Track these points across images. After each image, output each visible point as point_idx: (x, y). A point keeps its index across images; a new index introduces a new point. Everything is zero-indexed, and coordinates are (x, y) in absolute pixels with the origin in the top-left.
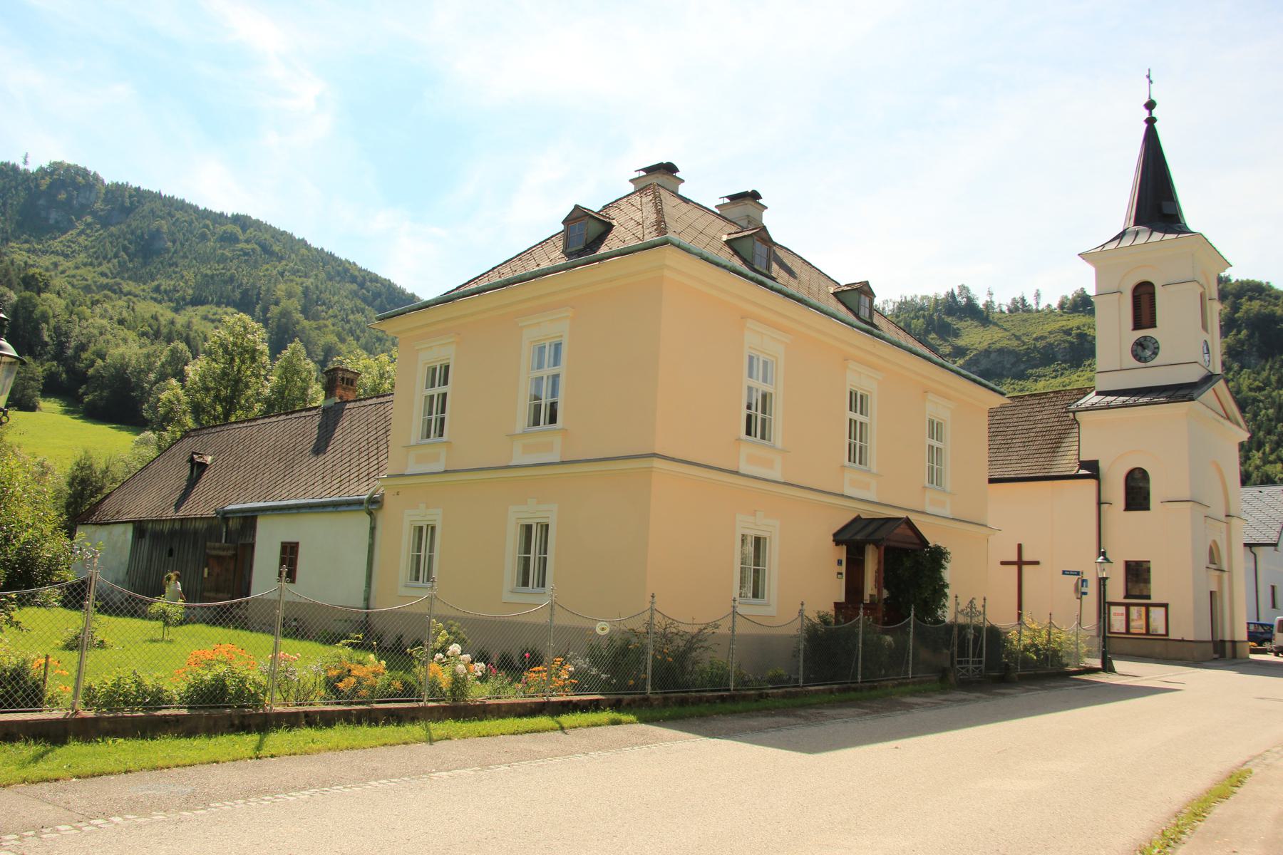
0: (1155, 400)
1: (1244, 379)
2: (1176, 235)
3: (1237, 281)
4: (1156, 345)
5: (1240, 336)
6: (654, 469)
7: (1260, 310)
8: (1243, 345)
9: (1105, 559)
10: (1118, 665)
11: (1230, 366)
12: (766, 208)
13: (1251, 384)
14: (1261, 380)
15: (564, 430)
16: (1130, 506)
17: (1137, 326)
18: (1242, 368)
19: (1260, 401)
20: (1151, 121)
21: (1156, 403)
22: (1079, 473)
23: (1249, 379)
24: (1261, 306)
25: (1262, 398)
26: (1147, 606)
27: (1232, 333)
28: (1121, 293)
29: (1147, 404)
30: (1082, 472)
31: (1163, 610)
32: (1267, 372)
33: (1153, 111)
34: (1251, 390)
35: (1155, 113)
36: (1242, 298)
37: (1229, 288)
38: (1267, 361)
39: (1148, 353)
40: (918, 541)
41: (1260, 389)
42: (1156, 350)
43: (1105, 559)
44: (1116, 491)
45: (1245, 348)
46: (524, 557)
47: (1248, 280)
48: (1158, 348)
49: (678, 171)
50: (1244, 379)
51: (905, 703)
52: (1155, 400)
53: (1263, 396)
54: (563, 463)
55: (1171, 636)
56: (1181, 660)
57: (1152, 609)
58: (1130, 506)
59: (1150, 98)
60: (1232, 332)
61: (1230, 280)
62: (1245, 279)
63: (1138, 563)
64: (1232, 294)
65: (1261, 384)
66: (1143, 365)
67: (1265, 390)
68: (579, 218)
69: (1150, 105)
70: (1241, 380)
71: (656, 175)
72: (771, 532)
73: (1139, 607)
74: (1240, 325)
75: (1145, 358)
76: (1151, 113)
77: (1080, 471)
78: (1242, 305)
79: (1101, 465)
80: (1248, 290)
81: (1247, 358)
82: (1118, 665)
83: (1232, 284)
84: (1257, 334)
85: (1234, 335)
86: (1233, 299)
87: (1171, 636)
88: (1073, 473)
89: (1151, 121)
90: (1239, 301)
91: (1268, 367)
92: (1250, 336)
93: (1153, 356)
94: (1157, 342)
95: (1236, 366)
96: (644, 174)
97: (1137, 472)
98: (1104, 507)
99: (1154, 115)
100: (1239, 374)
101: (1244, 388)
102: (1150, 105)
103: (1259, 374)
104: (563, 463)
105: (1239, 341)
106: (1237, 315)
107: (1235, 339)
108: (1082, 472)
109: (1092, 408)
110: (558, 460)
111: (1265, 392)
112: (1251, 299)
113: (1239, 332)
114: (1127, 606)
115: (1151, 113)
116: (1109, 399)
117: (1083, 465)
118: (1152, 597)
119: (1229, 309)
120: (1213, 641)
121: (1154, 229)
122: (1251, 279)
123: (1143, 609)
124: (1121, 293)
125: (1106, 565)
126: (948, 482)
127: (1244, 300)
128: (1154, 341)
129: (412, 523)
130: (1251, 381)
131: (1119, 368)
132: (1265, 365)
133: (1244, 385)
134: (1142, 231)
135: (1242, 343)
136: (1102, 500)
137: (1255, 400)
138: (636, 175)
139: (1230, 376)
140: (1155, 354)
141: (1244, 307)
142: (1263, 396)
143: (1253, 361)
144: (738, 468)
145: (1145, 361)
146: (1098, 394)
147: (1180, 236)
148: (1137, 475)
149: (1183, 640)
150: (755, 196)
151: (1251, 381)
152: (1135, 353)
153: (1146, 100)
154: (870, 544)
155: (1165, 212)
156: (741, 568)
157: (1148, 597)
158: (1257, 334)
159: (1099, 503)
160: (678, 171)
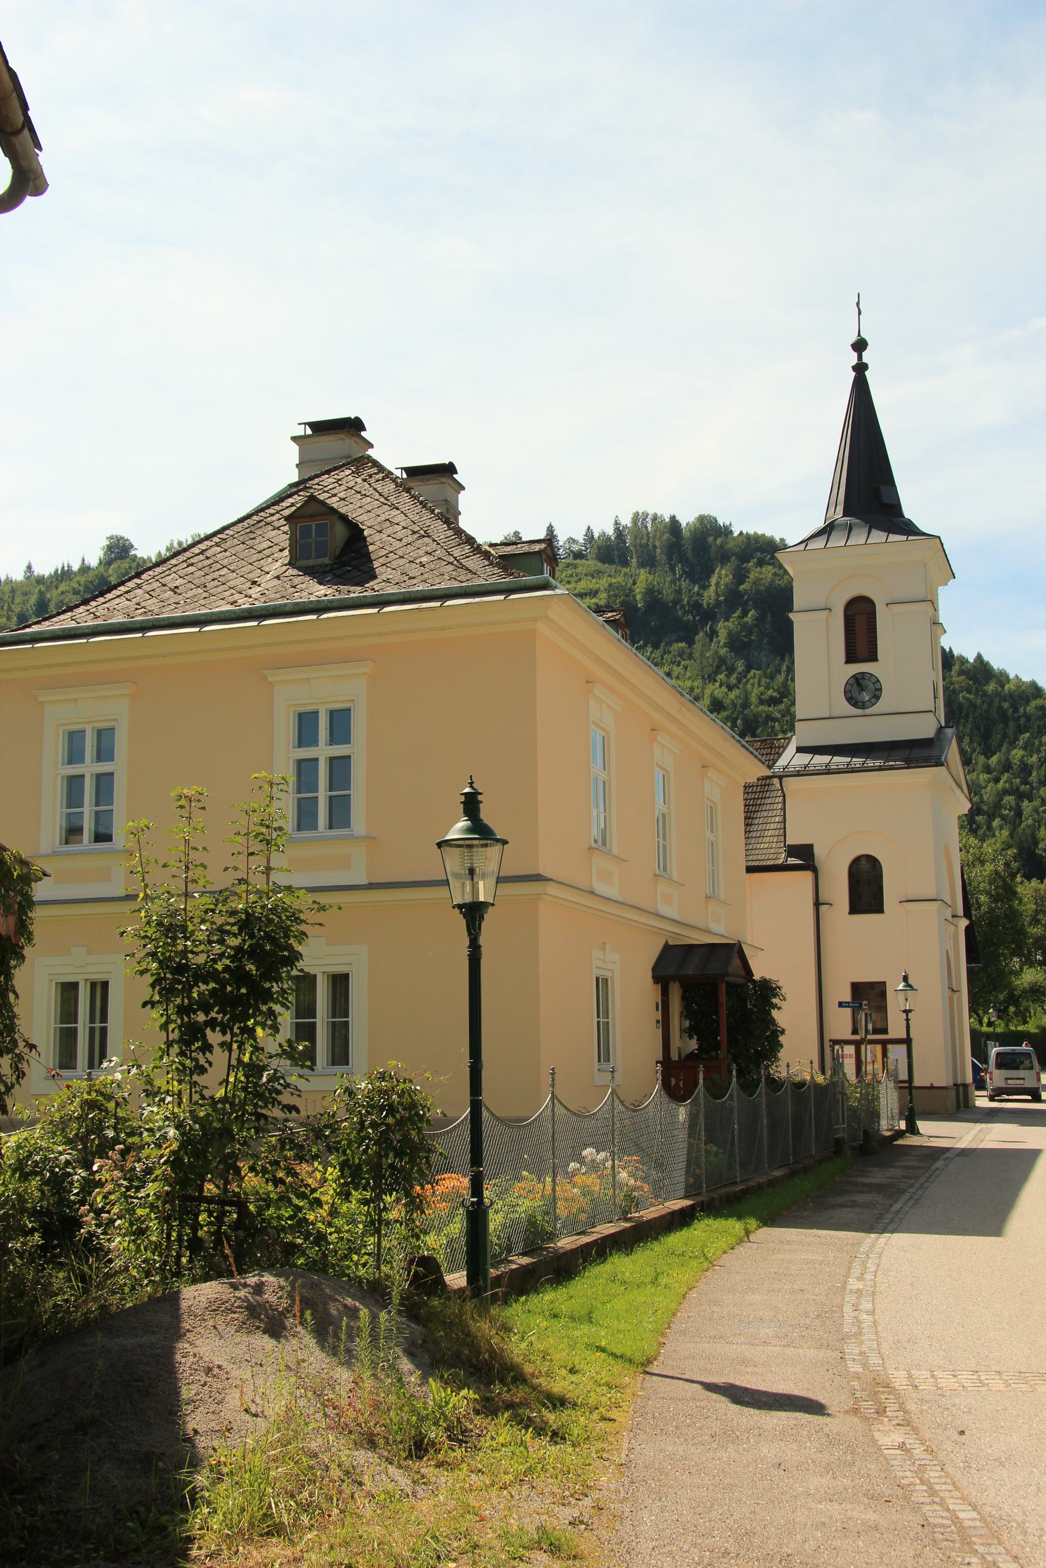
0: (890, 763)
1: (753, 685)
2: (904, 538)
3: (741, 533)
4: (877, 686)
5: (746, 619)
6: (543, 896)
7: (773, 581)
8: (751, 633)
9: (908, 985)
10: (922, 1125)
11: (733, 665)
12: (463, 488)
13: (762, 694)
14: (776, 687)
15: (370, 839)
16: (856, 908)
17: (851, 657)
18: (748, 668)
19: (774, 720)
20: (860, 368)
21: (892, 768)
22: (788, 863)
23: (759, 685)
24: (775, 574)
25: (778, 715)
26: (884, 1043)
27: (736, 615)
28: (830, 610)
29: (880, 769)
30: (792, 861)
31: (903, 1048)
32: (783, 675)
33: (864, 353)
34: (762, 702)
35: (866, 357)
36: (749, 562)
37: (731, 545)
38: (783, 659)
39: (866, 697)
40: (743, 973)
41: (773, 701)
42: (877, 693)
43: (908, 985)
44: (838, 889)
45: (753, 638)
46: (296, 1023)
47: (755, 533)
48: (881, 689)
49: (365, 430)
50: (753, 685)
51: (866, 1185)
52: (890, 763)
53: (779, 711)
54: (371, 886)
55: (917, 1083)
56: (929, 1114)
57: (889, 1046)
58: (856, 908)
59: (859, 335)
60: (735, 612)
61: (731, 532)
62: (751, 532)
63: (872, 985)
64: (735, 554)
65: (775, 694)
66: (859, 712)
67: (782, 702)
68: (316, 516)
69: (860, 346)
70: (749, 686)
71: (342, 436)
72: (613, 970)
73: (873, 1046)
74: (746, 602)
75: (863, 703)
76: (860, 357)
77: (789, 859)
78: (749, 573)
79: (816, 851)
80: (757, 550)
81: (756, 653)
82: (922, 1125)
83: (734, 539)
84: (769, 618)
85: (739, 617)
86: (736, 562)
87: (917, 1083)
88: (780, 862)
89: (860, 368)
90: (745, 565)
91: (784, 668)
92: (760, 620)
93: (873, 700)
94: (878, 681)
95: (740, 666)
96: (309, 432)
97: (863, 861)
98: (823, 909)
99: (864, 360)
100: (745, 676)
101: (753, 699)
102: (860, 346)
103: (772, 678)
104: (371, 886)
105: (744, 626)
106: (742, 587)
107: (739, 624)
108: (792, 861)
109: (803, 772)
110: (364, 881)
111: (782, 706)
112: (761, 563)
113: (745, 614)
114: (858, 1044)
115: (860, 357)
116: (825, 759)
117: (793, 851)
118: (889, 1030)
119: (731, 577)
120: (955, 1085)
121: (873, 525)
122: (760, 533)
123: (879, 1047)
124: (830, 610)
125: (910, 993)
126: (120, 831)
127: (751, 564)
128: (874, 680)
129: (52, 977)
130: (762, 688)
131: (828, 716)
132: (780, 665)
133: (753, 695)
134: (859, 526)
135: (748, 629)
136: (821, 900)
137: (769, 718)
138: (300, 431)
139: (733, 680)
140: (876, 697)
141: (752, 576)
142: (779, 711)
143: (764, 659)
144: (591, 886)
145: (863, 707)
146: (800, 750)
147: (910, 538)
148: (864, 865)
149: (932, 1087)
150: (448, 470)
151: (762, 688)
152: (849, 695)
153: (854, 338)
154: (674, 982)
155: (885, 501)
156: (347, 1016)
157: (885, 1031)
158: (769, 618)
159: (817, 904)
160: (365, 430)
